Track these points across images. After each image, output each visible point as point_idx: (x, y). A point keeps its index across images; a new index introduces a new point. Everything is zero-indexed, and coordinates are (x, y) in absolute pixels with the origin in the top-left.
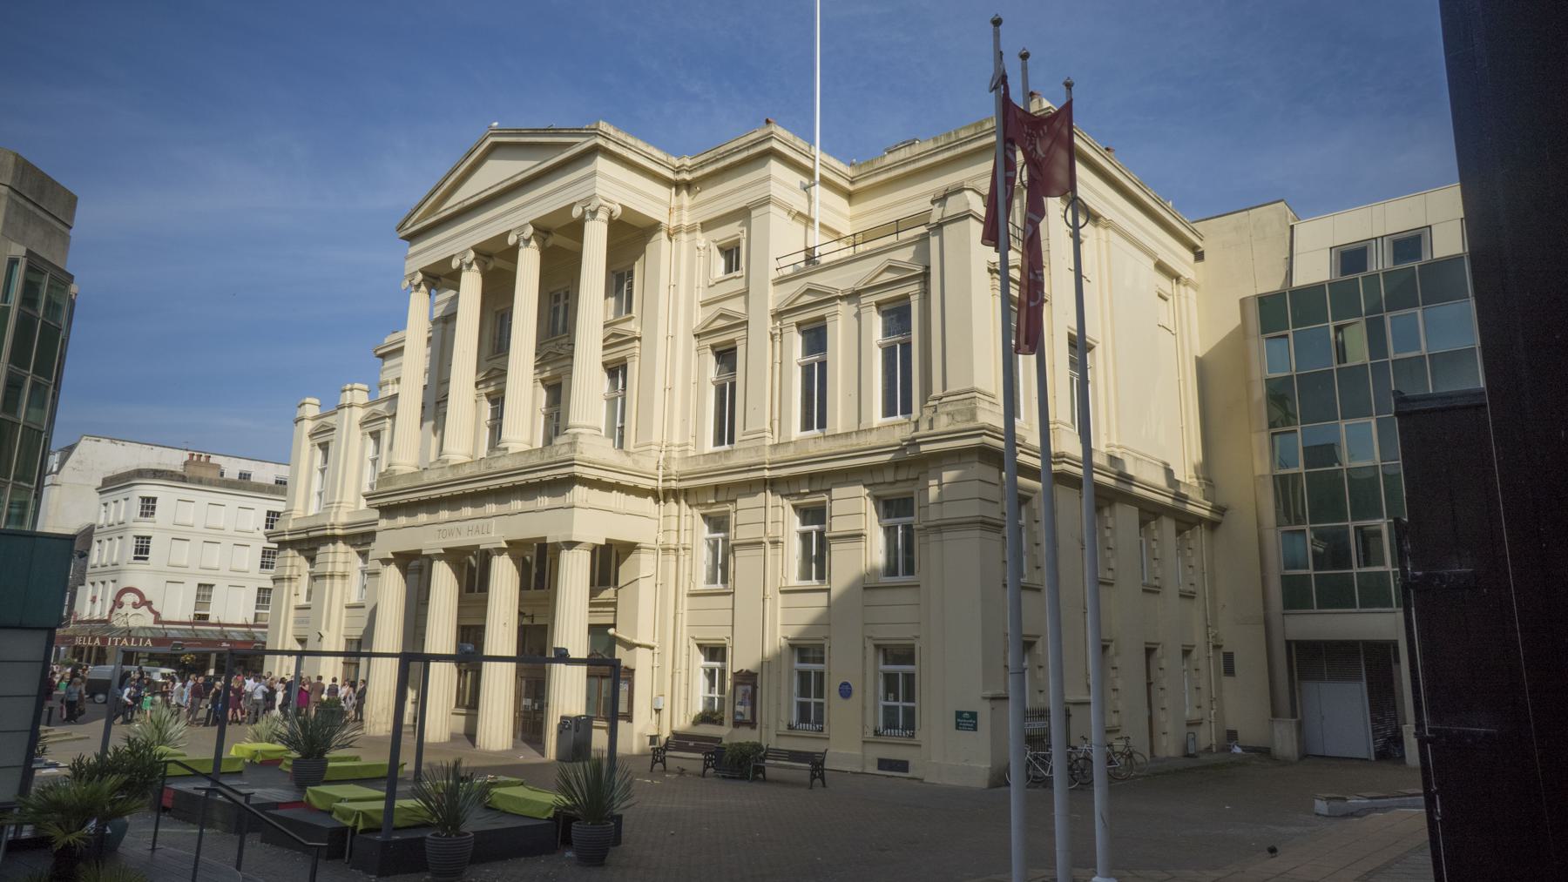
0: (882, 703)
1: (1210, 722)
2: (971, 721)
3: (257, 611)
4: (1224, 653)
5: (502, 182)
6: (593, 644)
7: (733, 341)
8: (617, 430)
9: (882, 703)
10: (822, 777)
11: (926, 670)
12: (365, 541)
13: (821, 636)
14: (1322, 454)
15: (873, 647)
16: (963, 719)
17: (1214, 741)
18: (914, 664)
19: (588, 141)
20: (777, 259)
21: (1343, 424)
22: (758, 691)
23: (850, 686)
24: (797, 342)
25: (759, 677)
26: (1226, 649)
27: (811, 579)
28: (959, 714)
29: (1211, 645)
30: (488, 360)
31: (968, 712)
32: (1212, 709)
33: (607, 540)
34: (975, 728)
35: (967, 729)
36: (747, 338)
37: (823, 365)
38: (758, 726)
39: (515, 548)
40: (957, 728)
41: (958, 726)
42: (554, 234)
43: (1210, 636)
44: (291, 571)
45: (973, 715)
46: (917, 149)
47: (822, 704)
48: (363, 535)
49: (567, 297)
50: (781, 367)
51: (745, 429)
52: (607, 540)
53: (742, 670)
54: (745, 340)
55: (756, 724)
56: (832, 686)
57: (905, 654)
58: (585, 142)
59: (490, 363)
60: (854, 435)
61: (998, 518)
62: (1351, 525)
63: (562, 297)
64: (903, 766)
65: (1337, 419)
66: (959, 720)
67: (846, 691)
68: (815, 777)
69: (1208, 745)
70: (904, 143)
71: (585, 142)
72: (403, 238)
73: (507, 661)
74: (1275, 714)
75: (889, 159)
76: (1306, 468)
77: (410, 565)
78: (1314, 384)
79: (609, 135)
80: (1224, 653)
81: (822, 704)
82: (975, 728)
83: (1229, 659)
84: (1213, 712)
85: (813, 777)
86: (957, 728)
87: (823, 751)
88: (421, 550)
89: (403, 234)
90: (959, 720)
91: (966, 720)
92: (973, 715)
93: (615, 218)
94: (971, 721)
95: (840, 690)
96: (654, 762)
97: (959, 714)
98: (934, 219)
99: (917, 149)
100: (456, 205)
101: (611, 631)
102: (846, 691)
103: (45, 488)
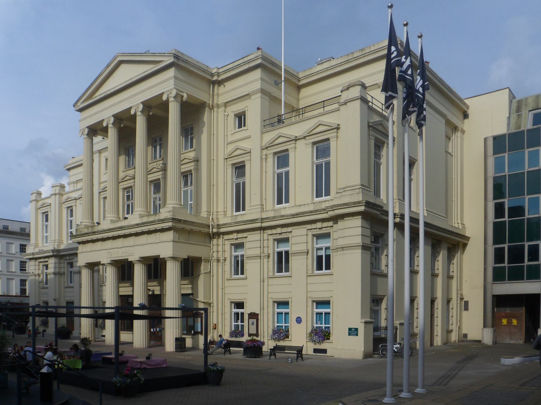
0: (233, 323)
1: (456, 330)
2: (355, 332)
3: (284, 313)
4: (464, 301)
5: (126, 81)
6: (183, 301)
7: (244, 162)
8: (189, 205)
9: (233, 323)
10: (302, 357)
11: (334, 310)
12: (71, 258)
13: (287, 297)
14: (517, 211)
15: (229, 302)
16: (352, 331)
17: (457, 339)
18: (244, 309)
19: (156, 66)
20: (264, 121)
21: (527, 198)
22: (259, 321)
23: (301, 319)
24: (271, 162)
25: (259, 315)
26: (465, 299)
27: (322, 269)
28: (350, 329)
29: (459, 298)
30: (123, 172)
31: (354, 328)
32: (458, 325)
33: (188, 256)
34: (357, 335)
35: (354, 335)
36: (250, 160)
37: (328, 164)
38: (259, 336)
39: (143, 260)
40: (349, 335)
41: (349, 334)
42: (124, 121)
43: (459, 294)
44: (39, 271)
45: (356, 330)
46: (333, 63)
47: (243, 325)
48: (70, 255)
49: (160, 140)
50: (227, 183)
51: (250, 204)
52: (188, 256)
53: (252, 313)
54: (250, 161)
55: (259, 335)
56: (293, 318)
57: (326, 303)
58: (167, 61)
59: (125, 173)
60: (303, 205)
61: (370, 244)
62: (527, 244)
63: (158, 140)
64: (324, 351)
65: (524, 195)
66: (350, 332)
67: (299, 320)
68: (299, 357)
69: (455, 340)
70: (326, 59)
71: (167, 61)
72: (77, 111)
73: (109, 309)
74: (485, 326)
75: (319, 68)
76: (508, 218)
77: (95, 268)
78: (516, 179)
79: (179, 57)
80: (464, 301)
81: (243, 325)
82: (357, 335)
83: (466, 303)
84: (458, 326)
85: (298, 357)
86: (349, 335)
87: (302, 346)
88: (100, 262)
89: (77, 108)
90: (350, 332)
91: (353, 332)
92: (356, 330)
93: (184, 100)
94: (355, 332)
95: (296, 320)
96: (271, 355)
97: (350, 329)
98: (342, 100)
99: (333, 63)
100: (103, 93)
101: (191, 296)
102: (299, 320)
103: (387, 44)
